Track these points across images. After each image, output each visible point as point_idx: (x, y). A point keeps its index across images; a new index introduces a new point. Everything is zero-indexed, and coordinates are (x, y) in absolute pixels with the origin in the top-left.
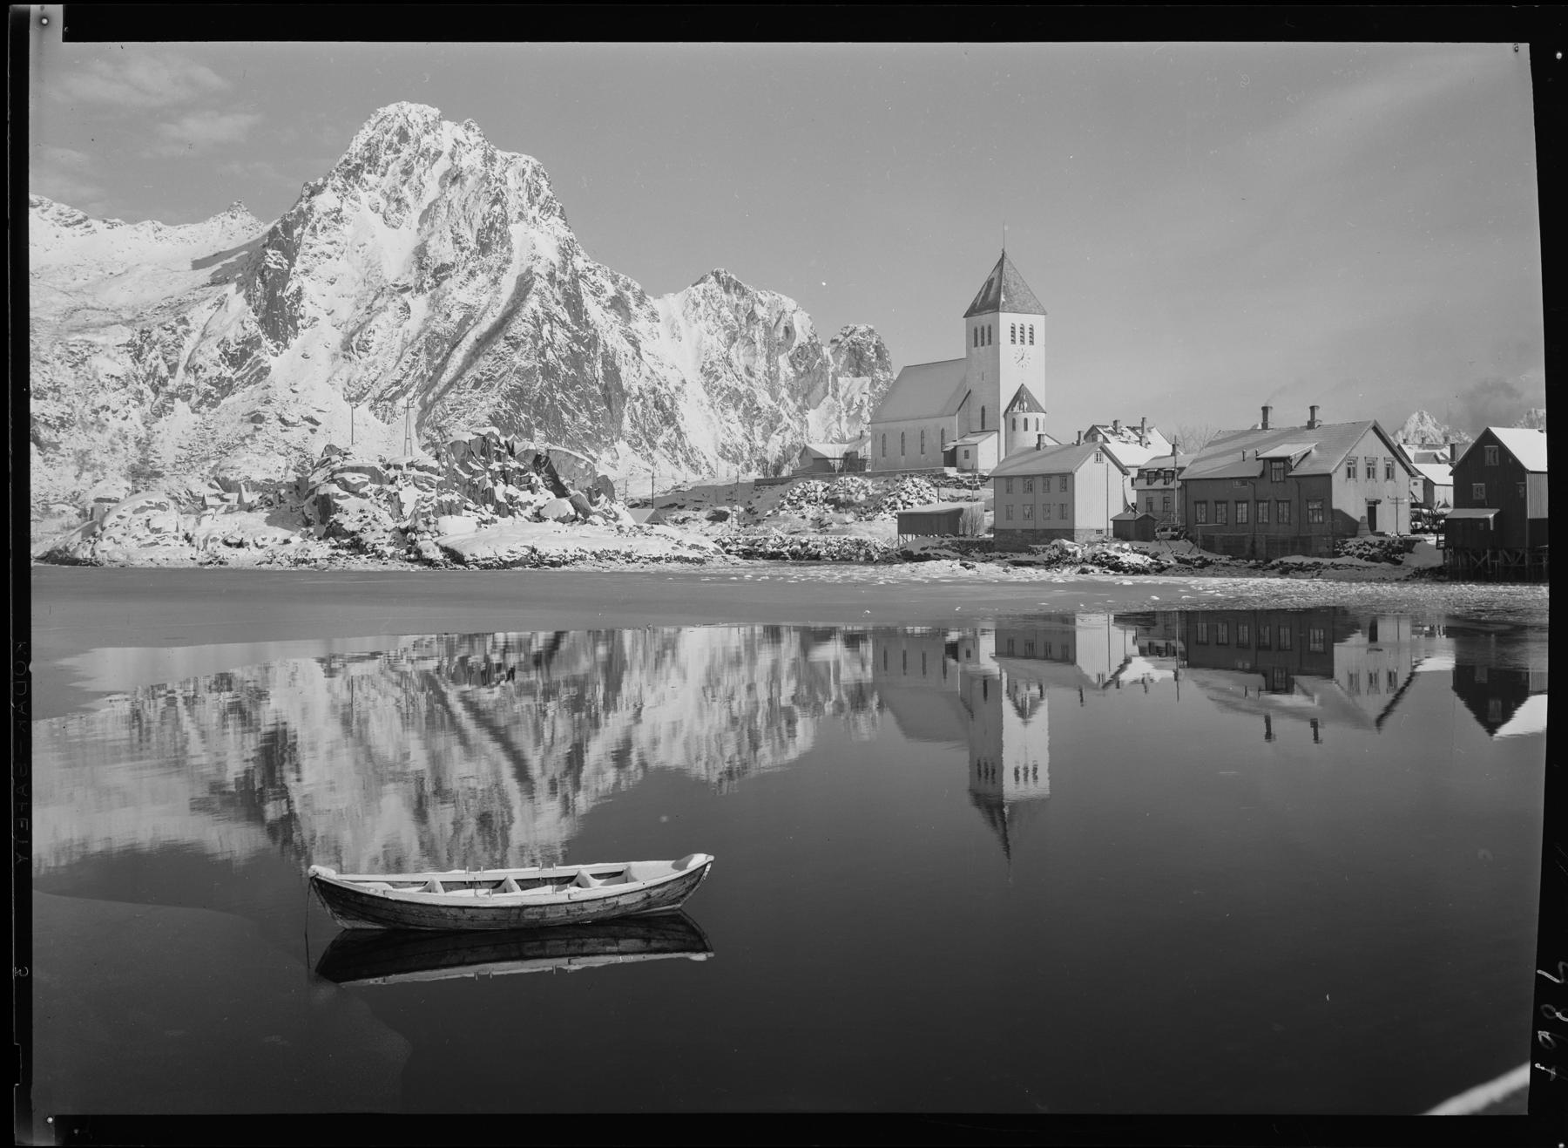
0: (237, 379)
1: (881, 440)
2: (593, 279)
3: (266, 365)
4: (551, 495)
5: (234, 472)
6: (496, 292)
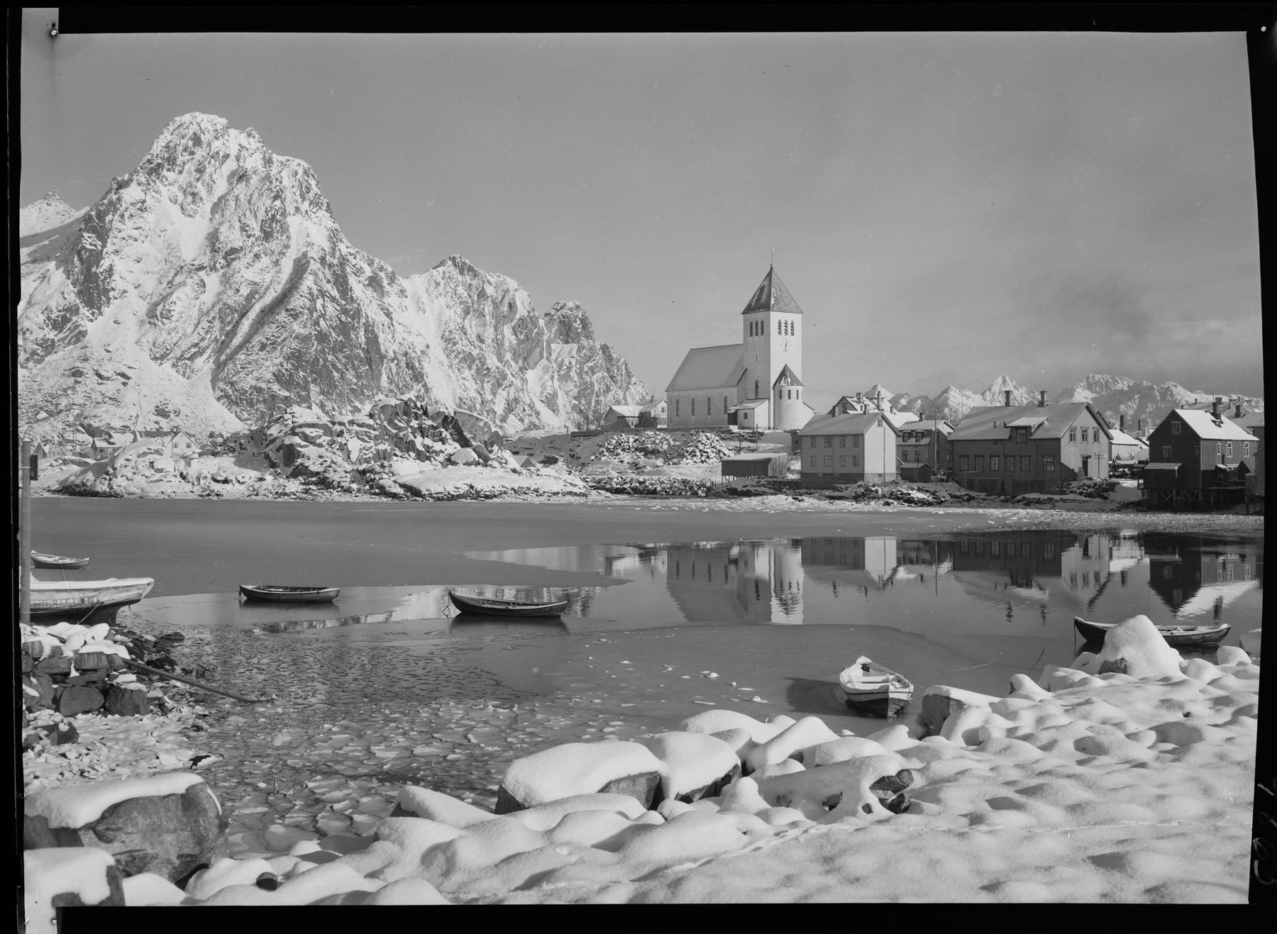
0: (59, 341)
1: (674, 405)
2: (354, 261)
3: (84, 329)
4: (457, 445)
5: (97, 420)
6: (277, 272)
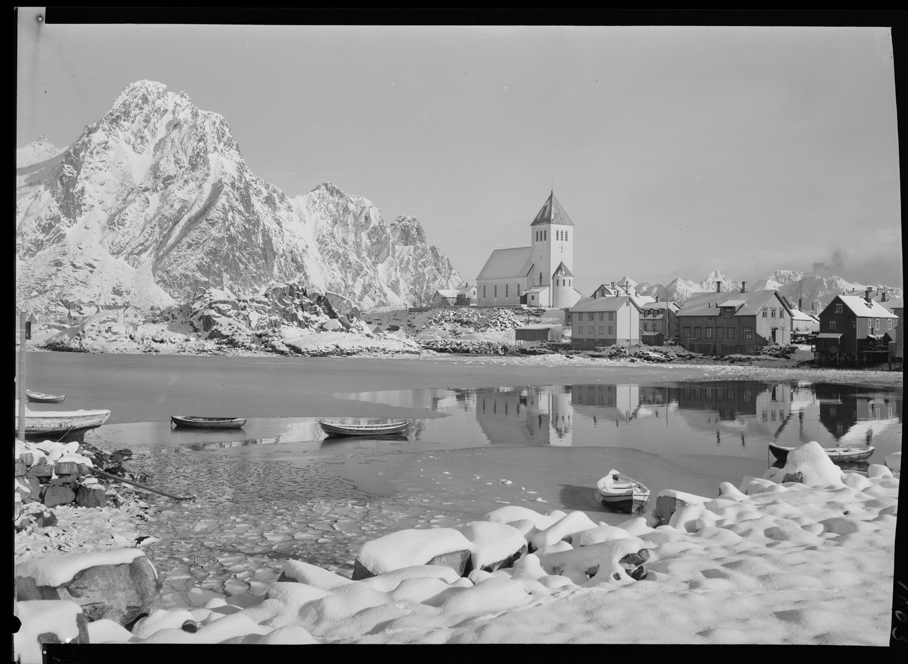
0: (46, 241)
1: (483, 289)
2: (255, 186)
3: (64, 233)
5: (72, 297)
6: (200, 193)
